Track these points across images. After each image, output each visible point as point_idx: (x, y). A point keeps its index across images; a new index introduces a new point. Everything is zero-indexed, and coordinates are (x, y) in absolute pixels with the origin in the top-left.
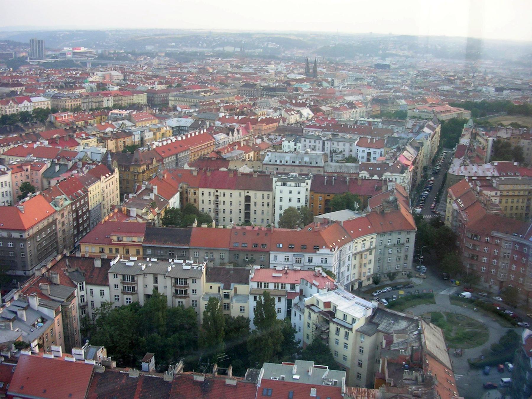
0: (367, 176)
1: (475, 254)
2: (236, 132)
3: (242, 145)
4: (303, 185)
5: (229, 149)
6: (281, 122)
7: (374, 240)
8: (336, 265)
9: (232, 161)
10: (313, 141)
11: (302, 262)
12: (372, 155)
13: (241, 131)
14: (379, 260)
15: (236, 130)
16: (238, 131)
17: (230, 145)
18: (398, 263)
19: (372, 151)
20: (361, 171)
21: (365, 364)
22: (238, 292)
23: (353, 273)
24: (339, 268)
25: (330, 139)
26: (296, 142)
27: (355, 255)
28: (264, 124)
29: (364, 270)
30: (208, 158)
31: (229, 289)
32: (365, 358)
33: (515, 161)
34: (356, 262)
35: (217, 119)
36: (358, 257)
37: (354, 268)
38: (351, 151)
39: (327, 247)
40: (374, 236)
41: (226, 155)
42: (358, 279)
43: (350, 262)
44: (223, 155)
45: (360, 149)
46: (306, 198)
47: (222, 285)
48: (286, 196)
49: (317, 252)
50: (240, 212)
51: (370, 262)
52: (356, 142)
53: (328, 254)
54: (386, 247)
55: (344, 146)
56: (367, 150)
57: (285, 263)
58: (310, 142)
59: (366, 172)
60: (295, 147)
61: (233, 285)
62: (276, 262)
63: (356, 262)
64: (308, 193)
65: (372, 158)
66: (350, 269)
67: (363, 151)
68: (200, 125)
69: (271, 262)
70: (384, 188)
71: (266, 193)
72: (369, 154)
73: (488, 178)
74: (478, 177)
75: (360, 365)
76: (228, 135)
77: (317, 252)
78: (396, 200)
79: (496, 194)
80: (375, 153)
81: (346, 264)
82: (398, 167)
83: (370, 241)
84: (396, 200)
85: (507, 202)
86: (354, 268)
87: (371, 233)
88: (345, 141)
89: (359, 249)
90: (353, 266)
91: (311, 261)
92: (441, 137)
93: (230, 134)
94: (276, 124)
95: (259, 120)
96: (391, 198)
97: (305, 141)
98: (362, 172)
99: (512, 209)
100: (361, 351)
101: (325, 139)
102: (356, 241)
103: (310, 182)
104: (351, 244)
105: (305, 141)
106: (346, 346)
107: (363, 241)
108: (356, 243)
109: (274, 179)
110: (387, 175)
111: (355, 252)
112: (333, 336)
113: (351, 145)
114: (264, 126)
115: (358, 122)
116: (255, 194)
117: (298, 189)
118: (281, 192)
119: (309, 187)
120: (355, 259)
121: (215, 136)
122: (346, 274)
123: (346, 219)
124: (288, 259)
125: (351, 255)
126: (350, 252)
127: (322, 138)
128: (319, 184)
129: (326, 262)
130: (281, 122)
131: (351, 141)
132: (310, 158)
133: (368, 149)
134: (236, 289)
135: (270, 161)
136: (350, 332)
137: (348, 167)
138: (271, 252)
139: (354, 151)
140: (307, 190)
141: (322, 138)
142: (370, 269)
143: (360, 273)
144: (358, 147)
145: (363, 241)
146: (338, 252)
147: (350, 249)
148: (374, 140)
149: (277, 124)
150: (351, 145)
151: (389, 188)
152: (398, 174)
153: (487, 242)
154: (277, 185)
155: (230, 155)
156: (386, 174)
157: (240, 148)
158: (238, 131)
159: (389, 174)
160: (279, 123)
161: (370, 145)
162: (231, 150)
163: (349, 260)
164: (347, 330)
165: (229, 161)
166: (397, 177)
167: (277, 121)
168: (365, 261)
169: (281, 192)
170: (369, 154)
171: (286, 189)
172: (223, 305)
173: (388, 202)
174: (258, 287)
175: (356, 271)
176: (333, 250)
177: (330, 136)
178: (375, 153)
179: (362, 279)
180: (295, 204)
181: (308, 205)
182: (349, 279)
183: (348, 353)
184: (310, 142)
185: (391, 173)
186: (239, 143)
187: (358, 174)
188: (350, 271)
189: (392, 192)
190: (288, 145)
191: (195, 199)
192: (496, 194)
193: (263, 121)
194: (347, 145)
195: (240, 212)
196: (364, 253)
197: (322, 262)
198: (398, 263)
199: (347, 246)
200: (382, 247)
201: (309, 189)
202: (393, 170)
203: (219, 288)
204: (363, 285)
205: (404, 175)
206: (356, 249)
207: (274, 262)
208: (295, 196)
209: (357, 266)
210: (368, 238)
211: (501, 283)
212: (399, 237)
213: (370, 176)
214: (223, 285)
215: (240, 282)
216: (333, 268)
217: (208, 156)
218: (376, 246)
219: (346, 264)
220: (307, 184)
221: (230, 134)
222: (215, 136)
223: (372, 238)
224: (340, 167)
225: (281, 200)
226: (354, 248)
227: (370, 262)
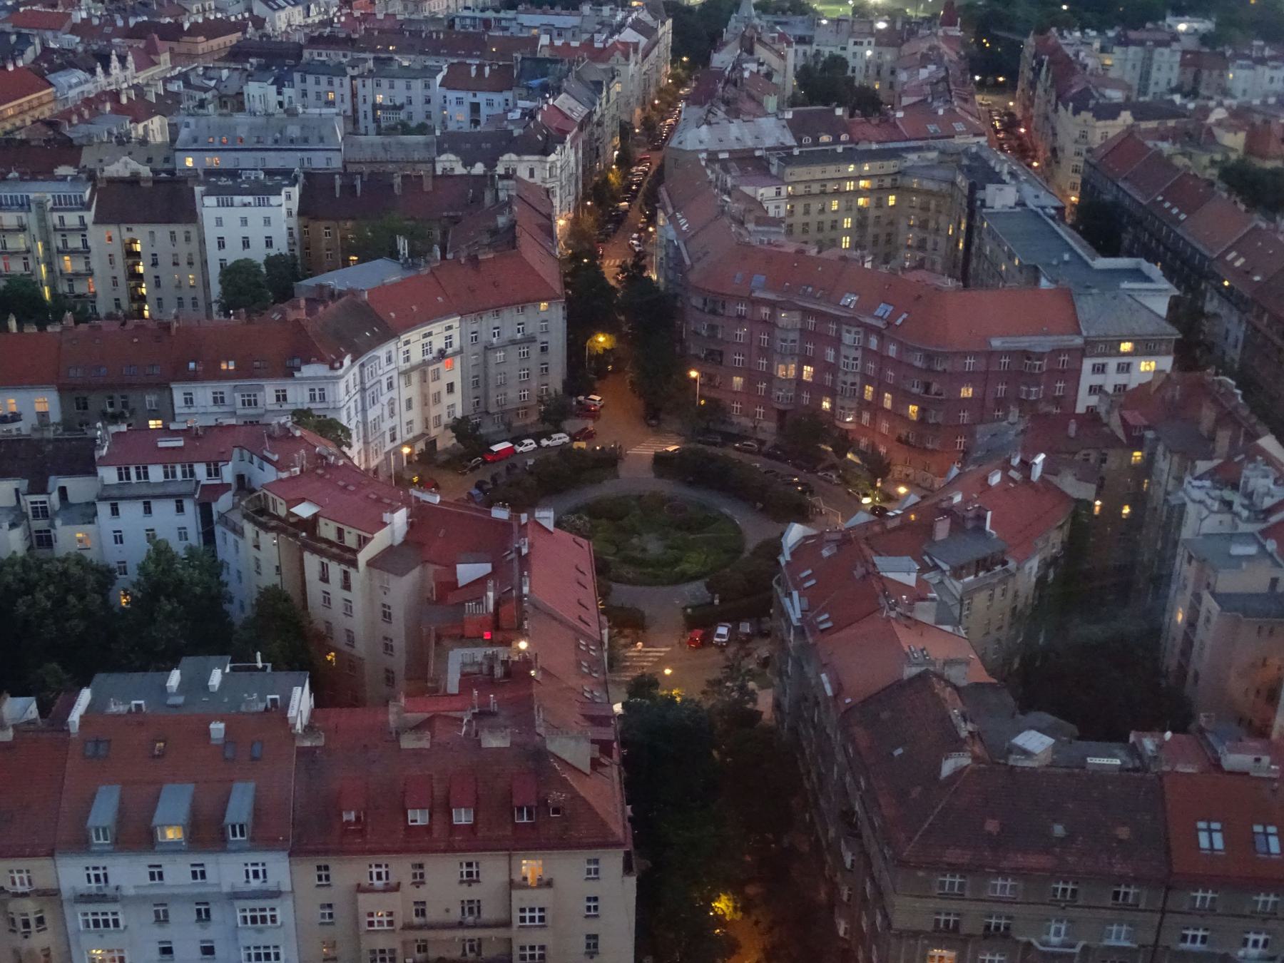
0: (459, 170)
1: (713, 347)
2: (115, 63)
3: (124, 100)
4: (274, 200)
5: (86, 114)
6: (250, 29)
7: (455, 333)
8: (352, 404)
9: (90, 144)
10: (324, 79)
11: (260, 403)
12: (484, 111)
13: (130, 58)
14: (478, 383)
15: (114, 57)
16: (123, 60)
17: (87, 102)
18: (525, 386)
19: (482, 98)
20: (440, 152)
21: (400, 643)
22: (72, 498)
23: (405, 421)
24: (364, 410)
25: (370, 71)
26: (279, 83)
27: (406, 373)
28: (201, 39)
29: (434, 411)
30: (23, 142)
31: (44, 491)
32: (398, 630)
33: (838, 106)
34: (412, 391)
35: (67, 26)
36: (415, 377)
37: (409, 407)
38: (428, 101)
39: (321, 360)
40: (455, 322)
41: (74, 131)
42: (423, 435)
43: (394, 393)
44: (66, 130)
45: (452, 95)
46: (291, 235)
47: (23, 484)
48: (233, 235)
49: (297, 375)
50: (115, 284)
51: (451, 388)
52: (439, 78)
53: (326, 378)
54: (489, 348)
55: (408, 88)
56: (468, 97)
57: (216, 409)
58: (318, 83)
59: (452, 157)
60: (280, 98)
61: (55, 482)
62: (193, 410)
63: (411, 391)
64: (294, 222)
65: (483, 119)
66: (397, 411)
67: (459, 101)
68: (13, 48)
69: (177, 411)
70: (488, 196)
71: (180, 229)
72: (475, 108)
73: (758, 153)
74: (730, 152)
75: (388, 648)
76: (93, 72)
77: (297, 375)
78: (512, 226)
79: (778, 194)
80: (490, 103)
81: (384, 399)
82: (540, 138)
83: (444, 332)
84: (512, 226)
85: (807, 212)
86: (409, 407)
87: (446, 314)
88: (409, 74)
89: (416, 357)
90: (404, 405)
91: (285, 398)
92: (676, 52)
93: (99, 70)
94: (233, 38)
95: (186, 26)
96: (502, 220)
97: (304, 80)
98: (444, 157)
99: (820, 229)
100: (387, 616)
101: (355, 72)
102: (404, 337)
103: (296, 191)
104: (391, 346)
105: (304, 80)
106: (348, 607)
107: (425, 336)
108: (407, 343)
109: (198, 190)
110: (508, 160)
111: (404, 366)
112: (315, 587)
113: (427, 86)
114: (203, 44)
115: (457, 21)
116: (152, 233)
117: (265, 211)
118: (219, 222)
119: (295, 204)
120: (408, 383)
121: (51, 77)
122: (386, 426)
123: (375, 283)
124: (222, 399)
125: (395, 374)
126: (393, 366)
127: (349, 70)
128: (319, 197)
129: (323, 397)
130: (250, 29)
131: (429, 73)
132: (302, 128)
133: (470, 94)
134: (63, 490)
135: (195, 140)
136: (352, 571)
137: (403, 145)
138: (173, 386)
139: (437, 102)
140: (290, 213)
141: (349, 70)
142: (455, 404)
143: (426, 420)
144: (443, 89)
145: (425, 336)
146: (356, 369)
147: (389, 360)
148: (487, 70)
149: (239, 34)
150: (427, 86)
151: (503, 195)
152: (536, 158)
153: (741, 317)
154: (209, 207)
155: (83, 129)
156: (506, 157)
157: (119, 110)
158: (123, 60)
159: (514, 157)
160: (245, 32)
161: (477, 85)
162: (91, 115)
163: (390, 386)
164: (344, 567)
165: (81, 147)
166: (534, 165)
167: (240, 26)
168: (433, 387)
169: (219, 222)
170: (475, 108)
171: (231, 215)
172: (34, 535)
173: (495, 232)
174: (121, 479)
175: (415, 414)
176: (337, 365)
177: (371, 64)
178: (490, 103)
179: (433, 432)
180: (258, 254)
181: (297, 253)
182: (398, 436)
183: (358, 623)
184: (318, 83)
185: (518, 154)
186: (115, 96)
187: (433, 162)
188: (396, 418)
189: (509, 203)
190: (260, 93)
191: (889, 235)
192: (778, 194)
193: (196, 30)
194: (418, 84)
195: (115, 284)
196: (431, 368)
197: (313, 398)
198: (525, 386)
199: (381, 352)
200: (478, 348)
201: (295, 210)
202: (524, 146)
203: (17, 491)
204: (439, 446)
205: (552, 157)
206: (408, 359)
207: (186, 411)
208: (257, 234)
209: (415, 404)
210: (437, 328)
211: (782, 414)
212: (522, 319)
213: (465, 166)
214: (26, 482)
215: (71, 473)
216: (344, 413)
217: (20, 136)
218: (461, 348)
219: (384, 399)
220: (289, 197)
221: (99, 70)
222: (51, 77)
223: (450, 328)
224: (385, 148)
225: (221, 243)
226: (401, 357)
227: (451, 388)
